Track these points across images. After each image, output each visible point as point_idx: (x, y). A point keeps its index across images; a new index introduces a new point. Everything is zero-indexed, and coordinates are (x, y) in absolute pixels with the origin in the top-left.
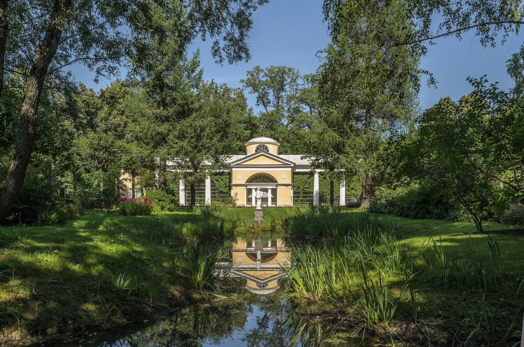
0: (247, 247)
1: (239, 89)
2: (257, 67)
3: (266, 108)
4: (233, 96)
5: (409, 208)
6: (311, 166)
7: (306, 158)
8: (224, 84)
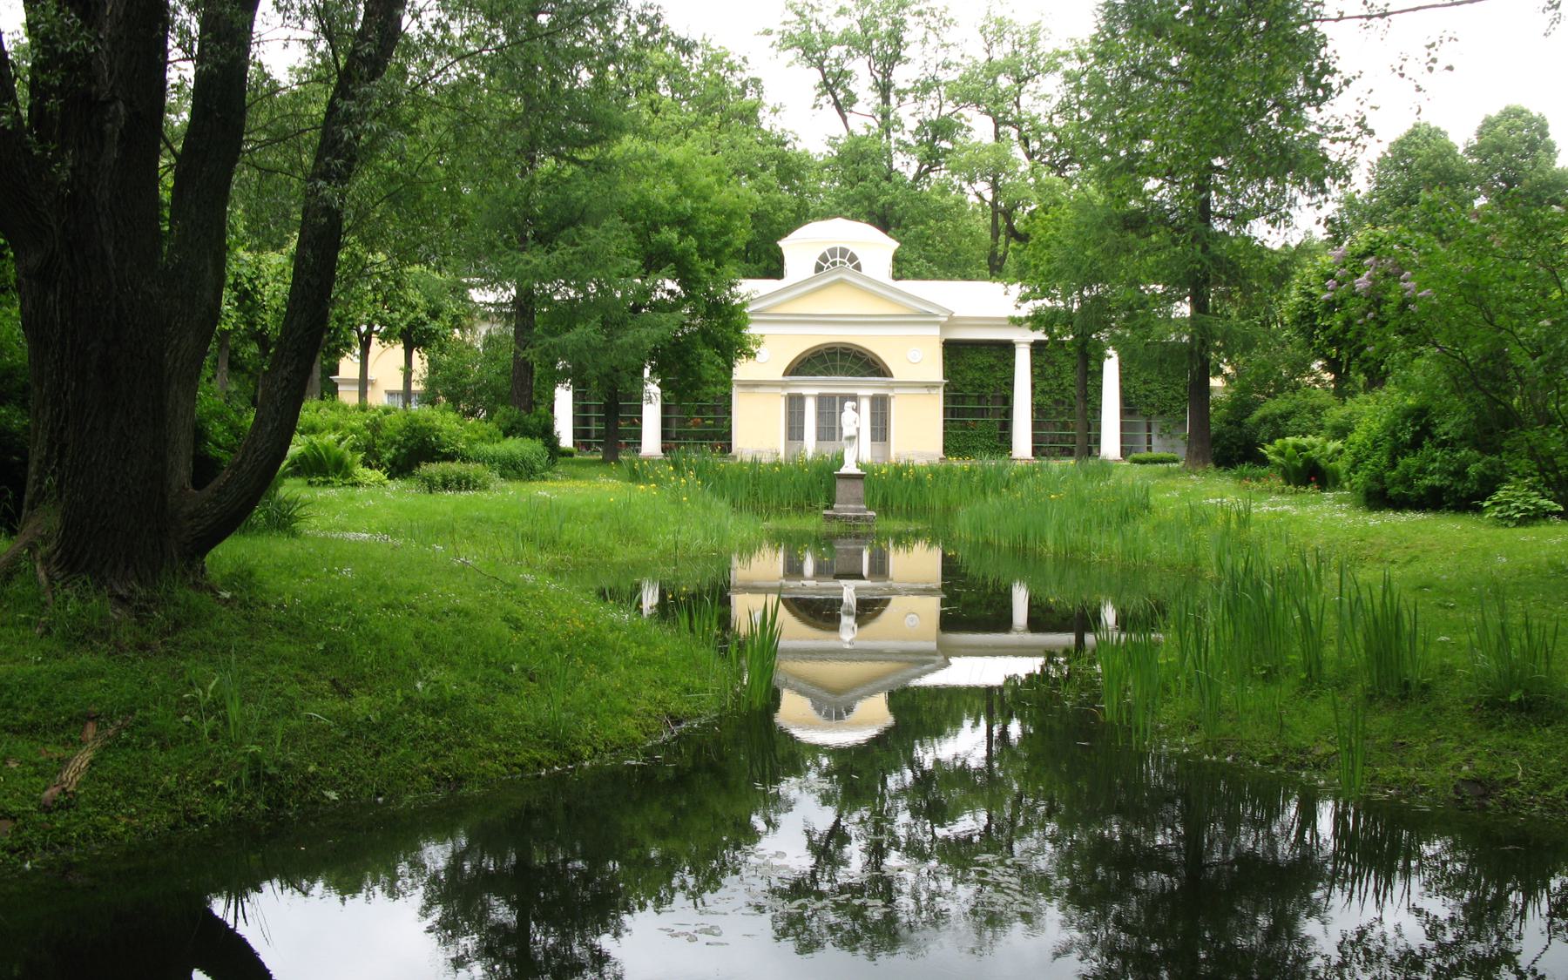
3: (844, 119)
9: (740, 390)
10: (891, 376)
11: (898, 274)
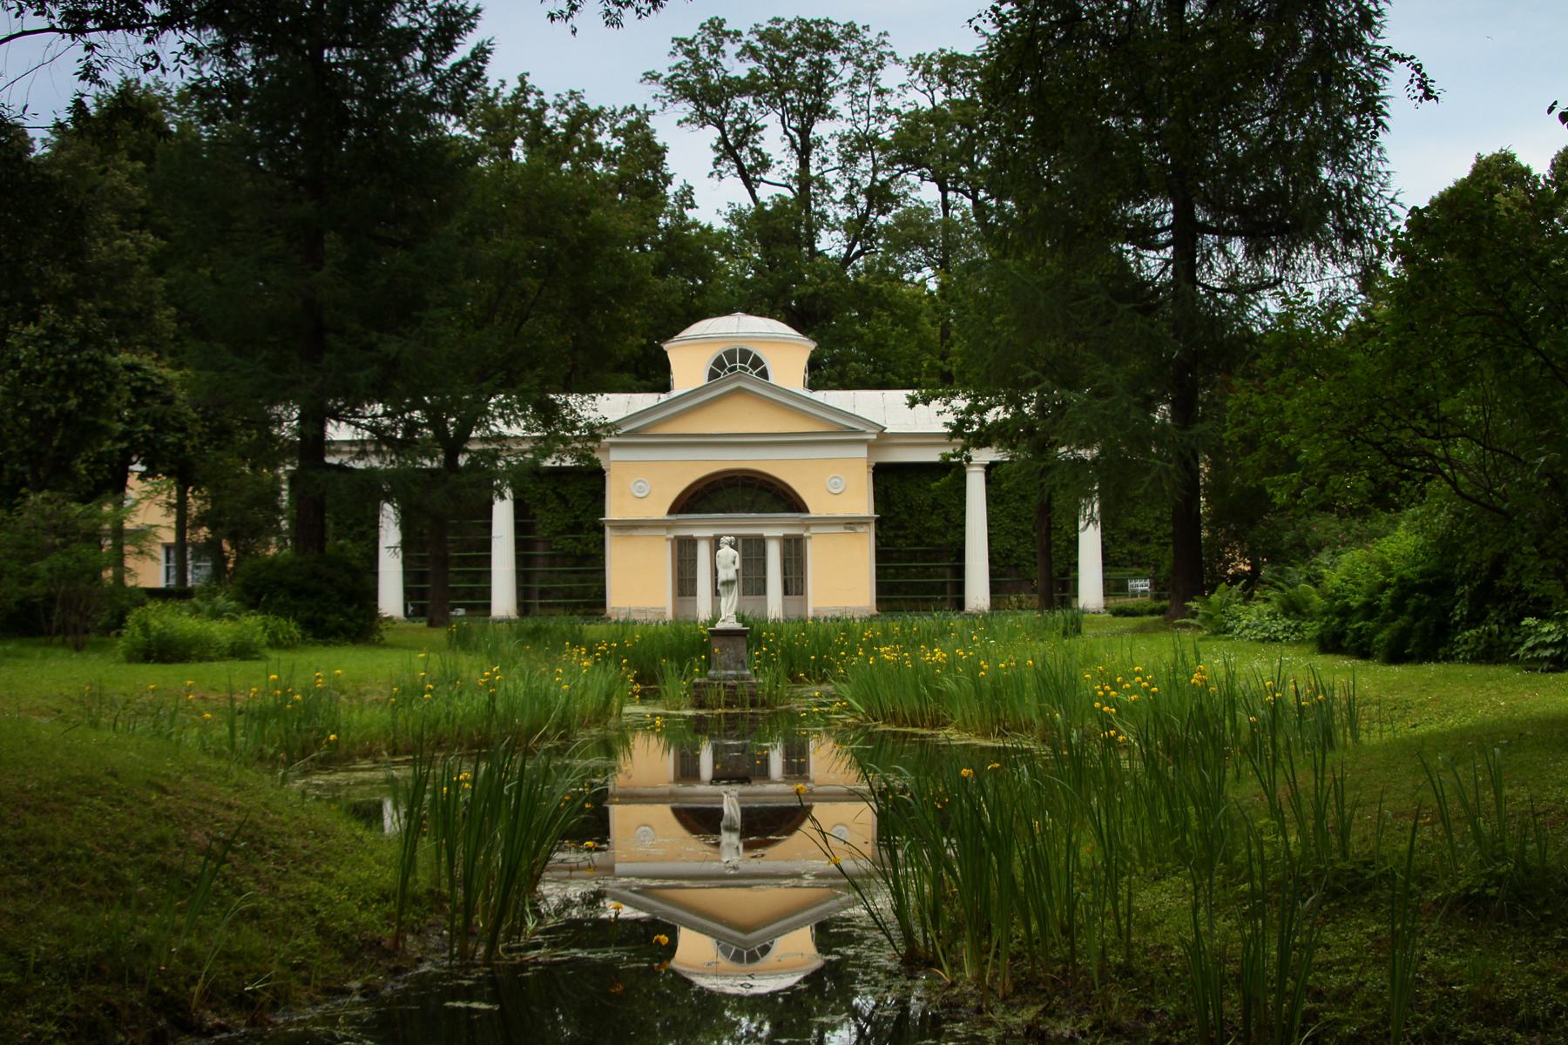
0: (677, 780)
1: (633, 108)
2: (711, 22)
4: (605, 139)
5: (1370, 610)
6: (950, 436)
7: (926, 403)
8: (572, 93)
9: (614, 533)
10: (807, 511)
11: (813, 385)
